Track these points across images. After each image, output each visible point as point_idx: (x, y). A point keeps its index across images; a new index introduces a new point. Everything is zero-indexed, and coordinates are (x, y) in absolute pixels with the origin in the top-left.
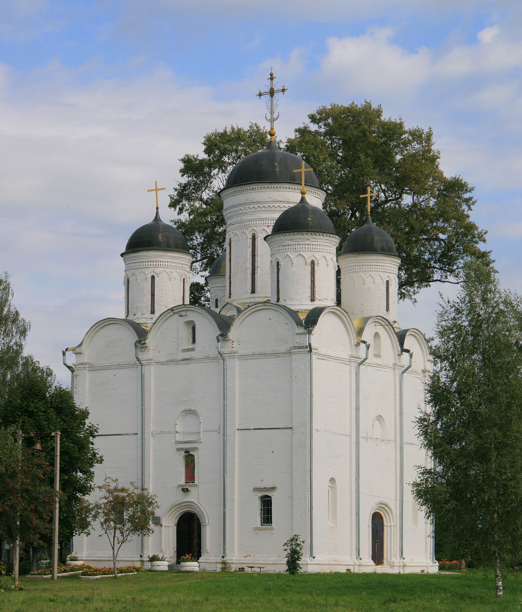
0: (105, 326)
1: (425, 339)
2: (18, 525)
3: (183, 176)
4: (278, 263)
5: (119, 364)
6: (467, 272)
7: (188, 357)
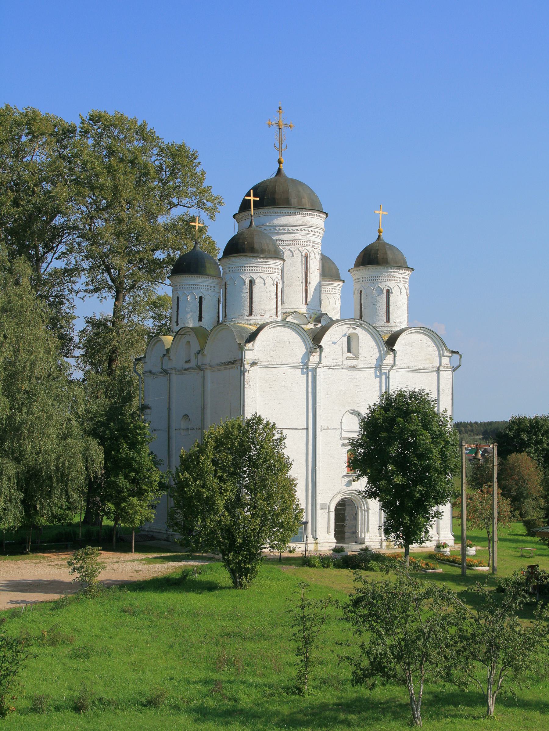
0: (220, 330)
1: (217, 326)
2: (400, 501)
3: (443, 512)
4: (178, 298)
5: (289, 364)
6: (101, 271)
7: (352, 365)
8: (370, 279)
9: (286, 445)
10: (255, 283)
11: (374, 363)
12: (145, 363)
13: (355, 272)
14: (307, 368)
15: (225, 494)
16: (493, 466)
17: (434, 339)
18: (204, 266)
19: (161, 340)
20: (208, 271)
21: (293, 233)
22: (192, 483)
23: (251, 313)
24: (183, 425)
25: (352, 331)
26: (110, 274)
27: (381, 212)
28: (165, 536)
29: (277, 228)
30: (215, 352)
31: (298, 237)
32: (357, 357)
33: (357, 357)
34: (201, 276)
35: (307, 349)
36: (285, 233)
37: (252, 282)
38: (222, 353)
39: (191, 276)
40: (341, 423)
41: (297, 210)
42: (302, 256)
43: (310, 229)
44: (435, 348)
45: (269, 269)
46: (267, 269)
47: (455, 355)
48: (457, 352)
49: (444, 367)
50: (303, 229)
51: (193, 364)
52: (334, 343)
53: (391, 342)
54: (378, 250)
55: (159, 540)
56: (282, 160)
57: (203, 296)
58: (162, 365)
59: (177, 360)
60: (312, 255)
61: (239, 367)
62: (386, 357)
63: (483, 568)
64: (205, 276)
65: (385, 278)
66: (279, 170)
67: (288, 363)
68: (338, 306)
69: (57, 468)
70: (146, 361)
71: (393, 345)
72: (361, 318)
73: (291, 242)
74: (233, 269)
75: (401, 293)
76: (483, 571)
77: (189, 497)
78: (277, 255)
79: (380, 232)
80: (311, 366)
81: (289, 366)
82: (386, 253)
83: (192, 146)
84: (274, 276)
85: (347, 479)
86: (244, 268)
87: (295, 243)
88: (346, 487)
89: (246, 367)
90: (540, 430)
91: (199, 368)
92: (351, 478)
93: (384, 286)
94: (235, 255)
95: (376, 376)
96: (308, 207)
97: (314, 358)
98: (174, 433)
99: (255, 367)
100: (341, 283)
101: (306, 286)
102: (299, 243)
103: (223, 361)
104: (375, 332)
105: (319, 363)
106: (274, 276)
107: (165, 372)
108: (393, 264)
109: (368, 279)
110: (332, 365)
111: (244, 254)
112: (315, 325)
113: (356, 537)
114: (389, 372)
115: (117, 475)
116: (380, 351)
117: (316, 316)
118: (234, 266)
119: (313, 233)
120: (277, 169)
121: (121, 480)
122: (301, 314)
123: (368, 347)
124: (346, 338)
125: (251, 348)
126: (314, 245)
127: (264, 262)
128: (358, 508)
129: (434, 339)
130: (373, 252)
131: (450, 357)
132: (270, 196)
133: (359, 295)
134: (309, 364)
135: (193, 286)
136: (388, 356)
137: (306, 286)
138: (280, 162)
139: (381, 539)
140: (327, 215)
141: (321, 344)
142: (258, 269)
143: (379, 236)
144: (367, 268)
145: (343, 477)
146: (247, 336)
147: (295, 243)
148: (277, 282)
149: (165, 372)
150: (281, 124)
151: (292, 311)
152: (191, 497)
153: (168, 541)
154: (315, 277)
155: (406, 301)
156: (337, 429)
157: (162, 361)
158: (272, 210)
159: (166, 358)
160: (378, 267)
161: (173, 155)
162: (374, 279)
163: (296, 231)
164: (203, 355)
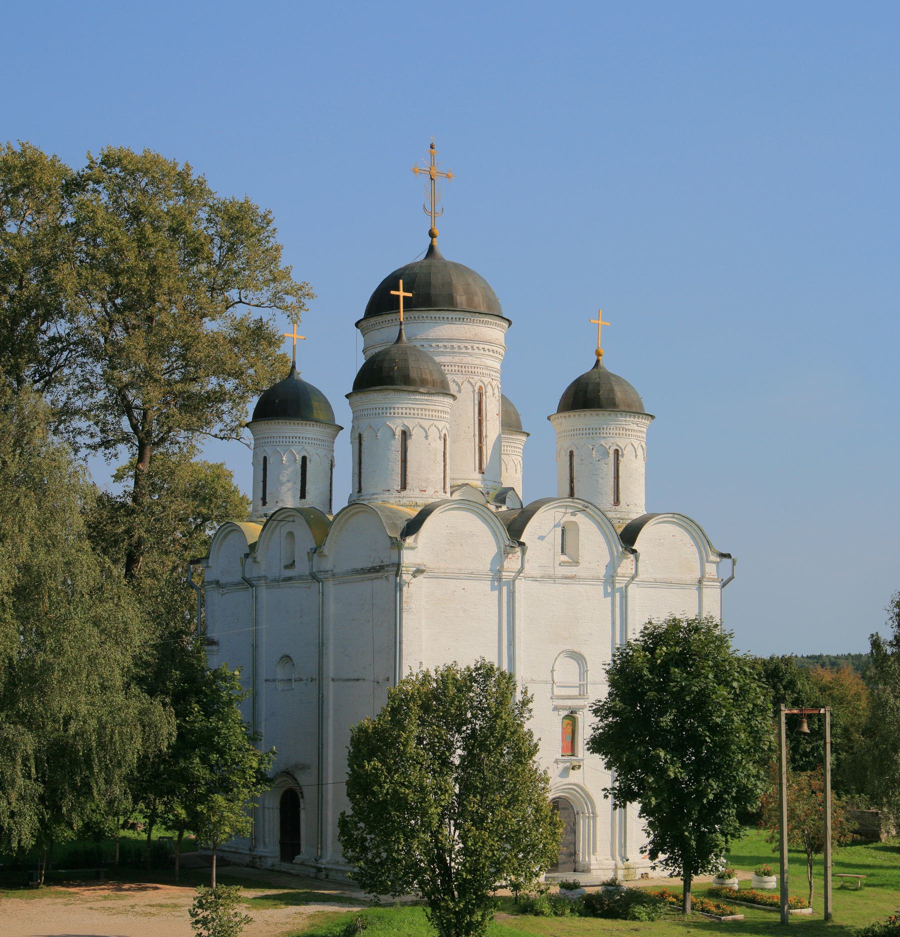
0: (354, 514)
4: (265, 458)
5: (472, 573)
7: (569, 574)
8: (588, 432)
9: (532, 713)
10: (411, 435)
11: (602, 572)
12: (208, 567)
13: (560, 420)
14: (500, 579)
15: (443, 797)
16: (825, 743)
17: (694, 534)
18: (309, 407)
19: (238, 530)
20: (315, 416)
21: (459, 353)
22: (386, 777)
23: (404, 487)
24: (280, 673)
25: (569, 518)
26: (130, 417)
27: (600, 322)
28: (247, 859)
29: (434, 345)
30: (342, 552)
31: (468, 359)
32: (576, 563)
33: (576, 563)
34: (304, 422)
35: (499, 548)
36: (454, 352)
37: (405, 434)
38: (365, 555)
39: (288, 422)
40: (552, 671)
41: (468, 314)
42: (474, 391)
43: (486, 347)
44: (695, 549)
45: (434, 413)
46: (431, 413)
47: (725, 560)
48: (728, 556)
49: (710, 580)
50: (475, 346)
51: (302, 567)
52: (542, 538)
53: (629, 536)
54: (598, 384)
55: (236, 864)
56: (436, 231)
57: (308, 457)
58: (243, 571)
59: (269, 563)
60: (489, 389)
61: (392, 578)
62: (621, 561)
63: (803, 910)
64: (312, 423)
65: (611, 431)
66: (431, 249)
67: (469, 571)
68: (519, 475)
69: (101, 745)
70: (210, 564)
71: (633, 543)
72: (572, 494)
73: (457, 368)
74: (374, 411)
75: (636, 456)
76: (805, 915)
77: (380, 803)
78: (442, 389)
79: (598, 354)
80: (507, 575)
81: (472, 576)
82: (612, 390)
83: (261, 204)
84: (440, 425)
85: (561, 766)
86: (392, 411)
87: (463, 369)
88: (561, 779)
89: (404, 577)
90: (781, 681)
91: (314, 577)
92: (568, 764)
93: (610, 444)
94: (377, 388)
95: (606, 595)
96: (483, 310)
97: (512, 563)
98: (263, 688)
99: (420, 577)
100: (524, 438)
101: (480, 441)
102: (470, 370)
103: (359, 567)
104: (603, 521)
105: (520, 571)
106: (440, 425)
107: (248, 583)
108: (622, 408)
109: (584, 432)
110: (539, 576)
111: (394, 387)
112: (497, 507)
113: (575, 862)
114: (626, 587)
115: (187, 758)
116: (611, 553)
117: (497, 492)
118: (375, 406)
119: (491, 353)
120: (427, 247)
121: (198, 769)
122: (476, 488)
123: (594, 545)
124: (560, 529)
125: (413, 545)
126: (492, 373)
127: (426, 400)
128: (578, 813)
129: (694, 534)
130: (591, 387)
131: (717, 563)
132: (416, 291)
133: (568, 458)
134: (504, 573)
135: (291, 440)
136: (625, 561)
137: (480, 441)
138: (432, 235)
139: (616, 865)
140: (510, 322)
141: (522, 540)
142: (416, 412)
143: (598, 361)
144: (583, 414)
145: (556, 761)
146: (402, 524)
147: (463, 369)
148: (445, 435)
149: (248, 583)
150: (433, 172)
151: (460, 482)
152: (385, 801)
153: (253, 867)
154: (493, 427)
155: (642, 470)
156: (546, 682)
157: (243, 565)
158: (425, 314)
159: (249, 560)
160: (601, 413)
161: (232, 220)
162: (594, 431)
163: (464, 350)
164: (322, 555)
